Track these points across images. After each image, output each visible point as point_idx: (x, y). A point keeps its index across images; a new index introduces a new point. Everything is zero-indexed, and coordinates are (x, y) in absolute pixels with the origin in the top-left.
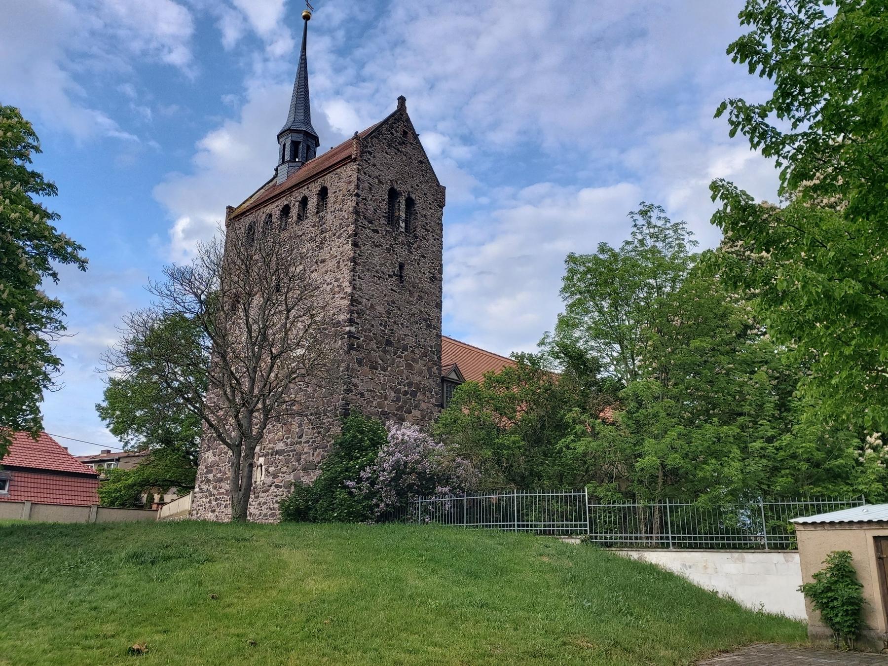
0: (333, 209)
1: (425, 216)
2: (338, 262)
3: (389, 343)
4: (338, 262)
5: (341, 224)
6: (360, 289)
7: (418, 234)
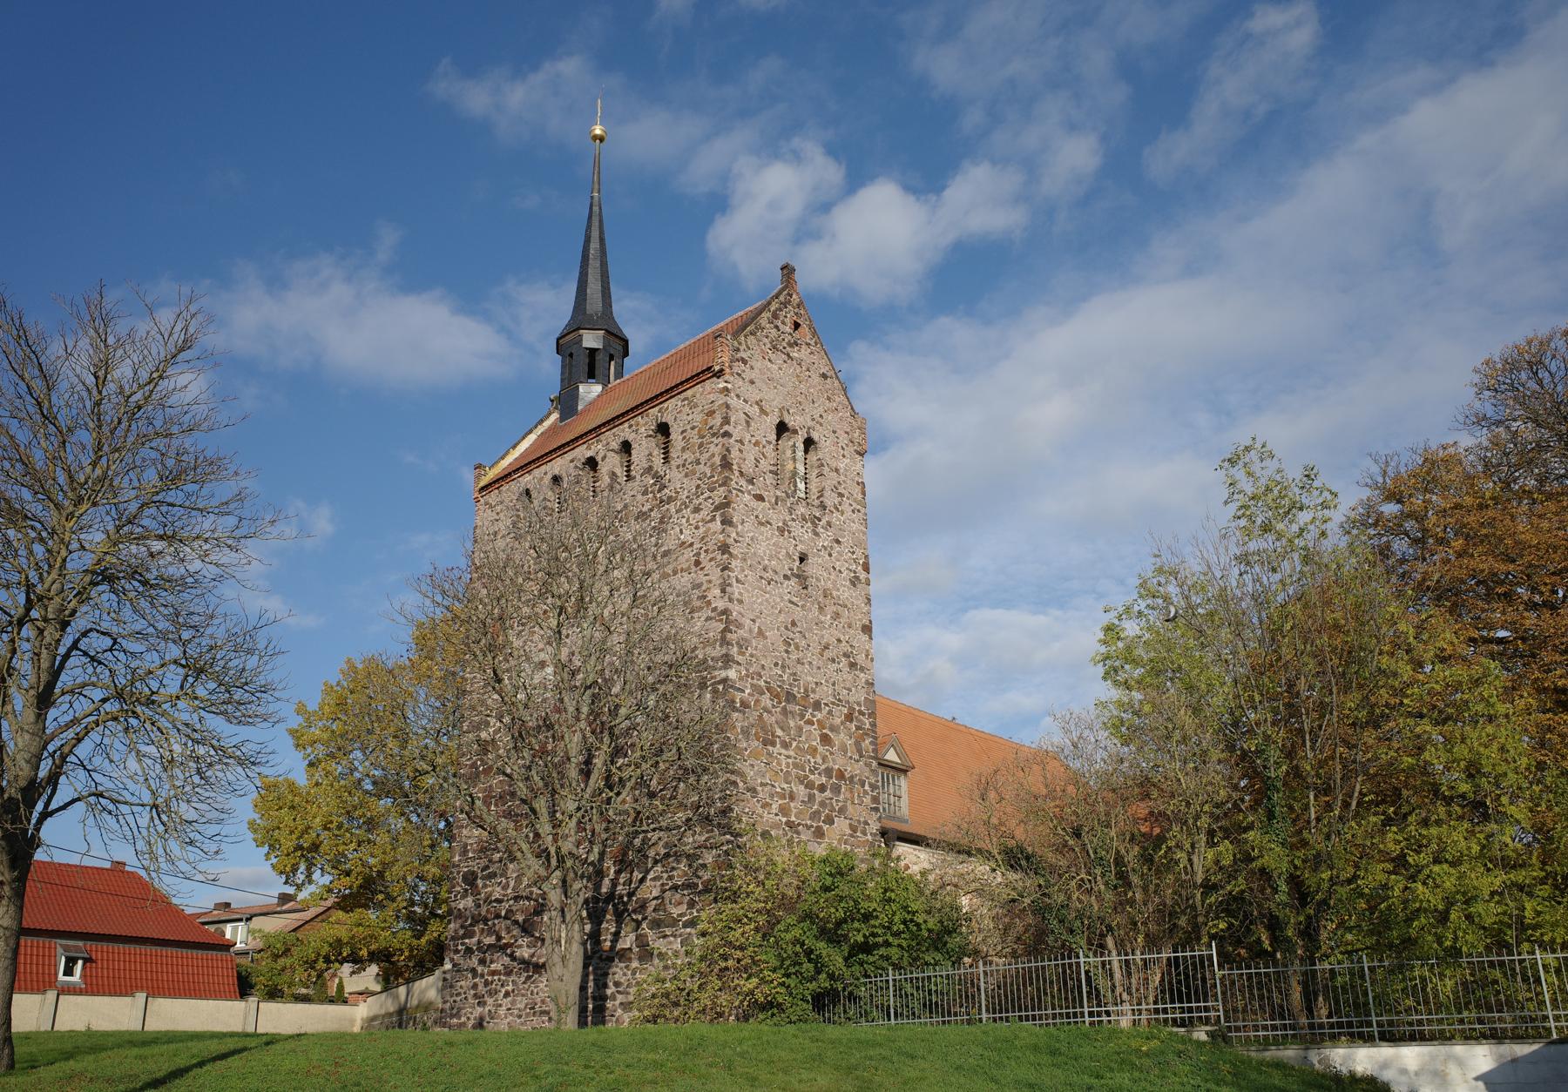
0: (680, 462)
1: (837, 470)
2: (698, 554)
3: (790, 697)
4: (698, 554)
5: (698, 487)
6: (740, 602)
7: (828, 503)
